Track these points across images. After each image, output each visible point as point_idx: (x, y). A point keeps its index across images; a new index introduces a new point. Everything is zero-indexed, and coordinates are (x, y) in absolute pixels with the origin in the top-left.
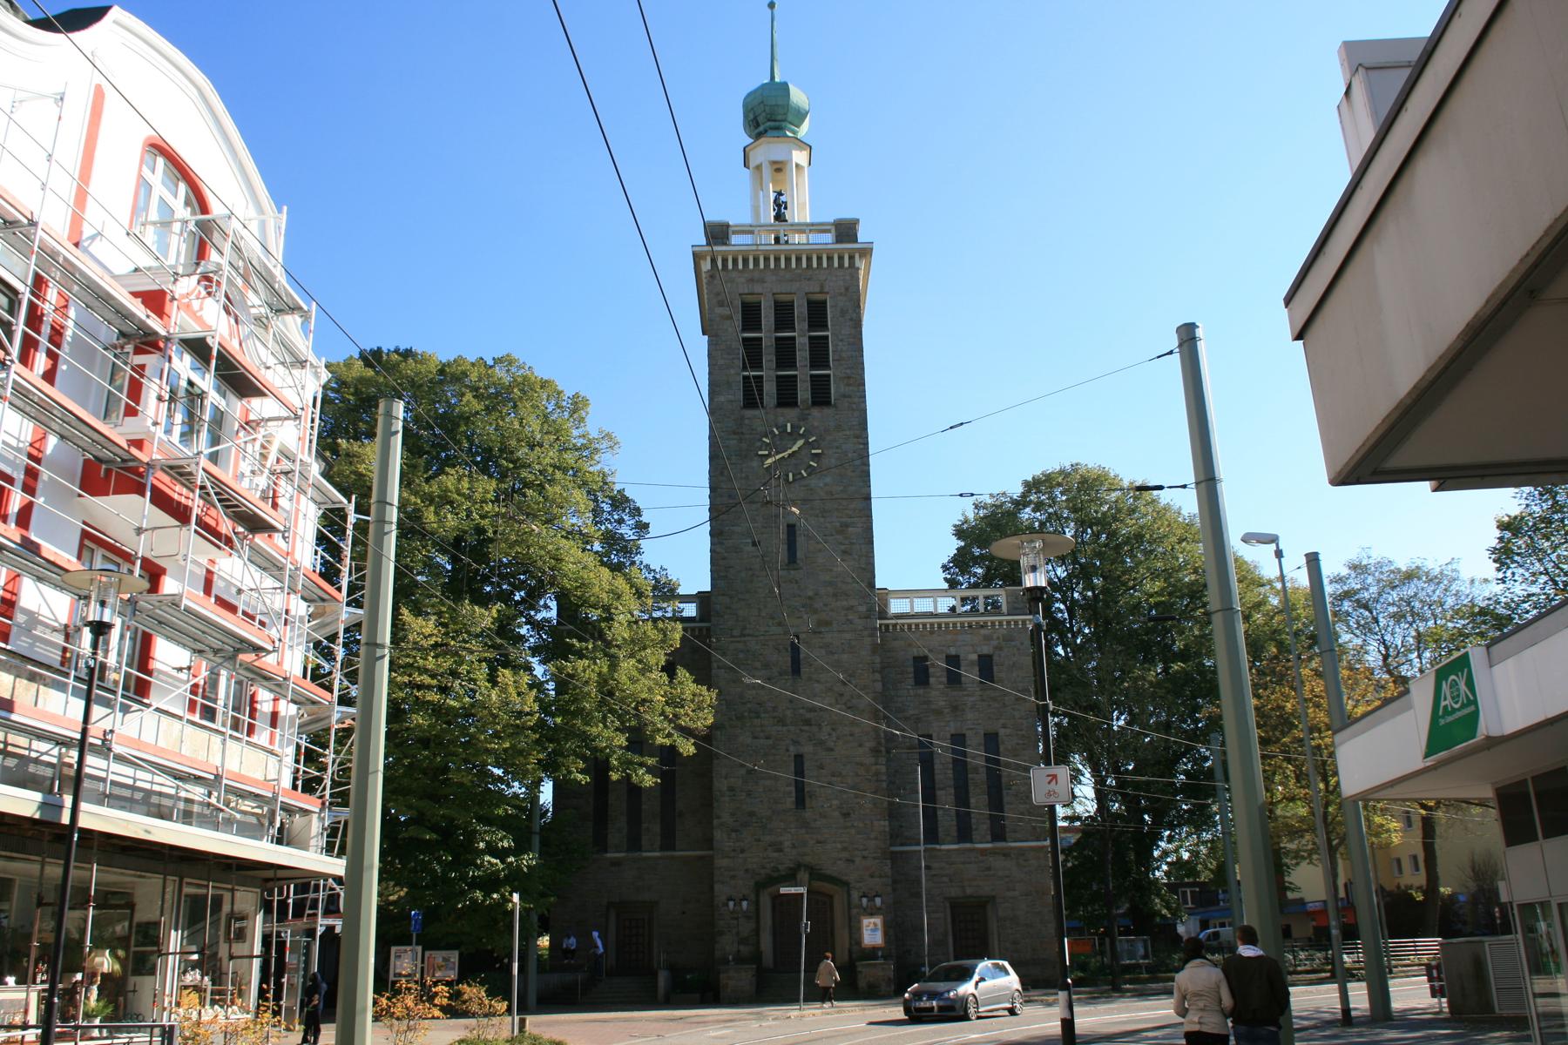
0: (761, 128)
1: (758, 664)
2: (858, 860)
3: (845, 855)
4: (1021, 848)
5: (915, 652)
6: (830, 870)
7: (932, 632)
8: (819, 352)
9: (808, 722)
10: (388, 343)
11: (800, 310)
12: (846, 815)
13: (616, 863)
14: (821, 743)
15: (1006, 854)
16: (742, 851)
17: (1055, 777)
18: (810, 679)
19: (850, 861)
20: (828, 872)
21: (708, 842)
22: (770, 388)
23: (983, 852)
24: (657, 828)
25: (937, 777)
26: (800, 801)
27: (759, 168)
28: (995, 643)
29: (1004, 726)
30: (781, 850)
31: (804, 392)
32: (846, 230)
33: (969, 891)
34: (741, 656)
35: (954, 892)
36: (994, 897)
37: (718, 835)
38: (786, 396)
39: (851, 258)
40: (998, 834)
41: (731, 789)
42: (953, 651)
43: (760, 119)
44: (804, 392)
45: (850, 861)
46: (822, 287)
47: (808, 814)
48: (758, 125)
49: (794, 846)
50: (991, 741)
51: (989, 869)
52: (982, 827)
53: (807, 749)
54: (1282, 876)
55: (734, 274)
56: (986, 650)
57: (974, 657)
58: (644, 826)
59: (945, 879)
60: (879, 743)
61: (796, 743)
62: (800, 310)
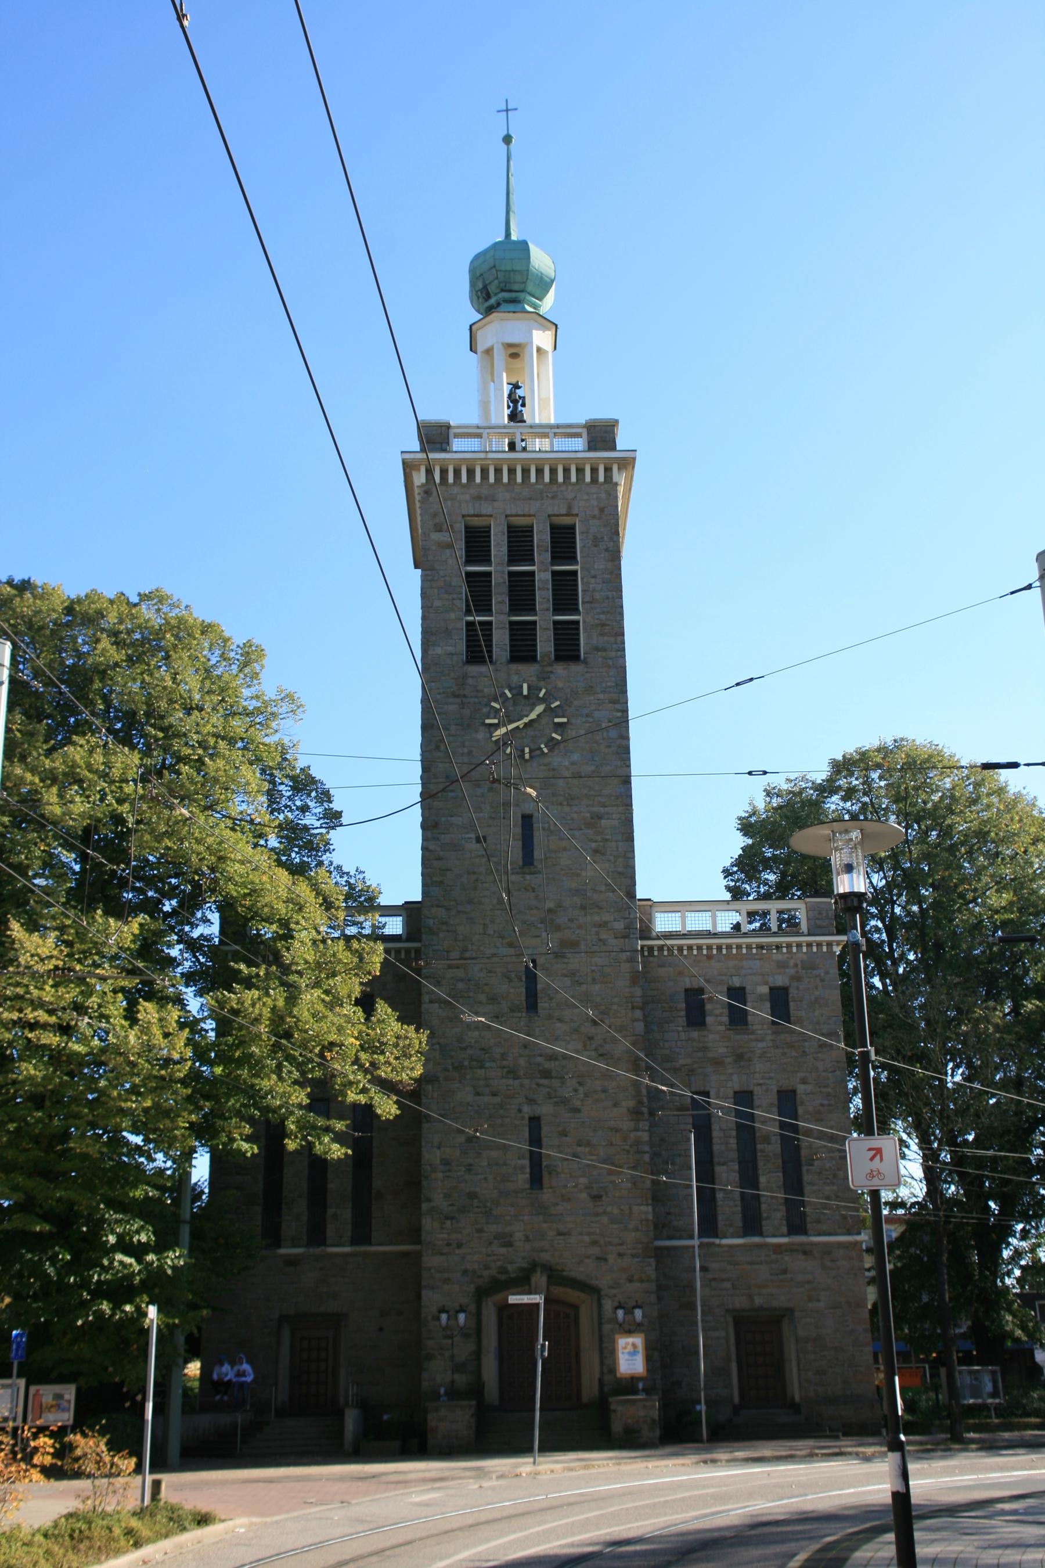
0: (493, 301)
1: (482, 997)
2: (611, 1258)
3: (595, 1251)
5: (688, 983)
7: (709, 957)
8: (565, 591)
9: (546, 1074)
11: (541, 537)
13: (292, 1262)
15: (806, 1251)
16: (460, 1246)
17: (879, 1151)
18: (550, 1017)
20: (573, 1274)
21: (415, 1234)
22: (501, 638)
23: (778, 1249)
24: (347, 1214)
25: (716, 1148)
27: (489, 352)
28: (791, 971)
29: (804, 1081)
30: (509, 1244)
31: (545, 644)
32: (602, 435)
33: (758, 1301)
34: (460, 986)
35: (740, 1302)
36: (791, 1310)
37: (427, 1223)
38: (523, 648)
39: (608, 470)
42: (736, 982)
43: (492, 289)
44: (545, 644)
46: (570, 507)
47: (546, 1196)
48: (488, 297)
49: (527, 1239)
50: (787, 1101)
51: (785, 1271)
53: (545, 1110)
55: (456, 490)
56: (780, 981)
57: (764, 990)
58: (330, 1211)
59: (728, 1285)
60: (640, 1102)
61: (531, 1101)
62: (541, 537)
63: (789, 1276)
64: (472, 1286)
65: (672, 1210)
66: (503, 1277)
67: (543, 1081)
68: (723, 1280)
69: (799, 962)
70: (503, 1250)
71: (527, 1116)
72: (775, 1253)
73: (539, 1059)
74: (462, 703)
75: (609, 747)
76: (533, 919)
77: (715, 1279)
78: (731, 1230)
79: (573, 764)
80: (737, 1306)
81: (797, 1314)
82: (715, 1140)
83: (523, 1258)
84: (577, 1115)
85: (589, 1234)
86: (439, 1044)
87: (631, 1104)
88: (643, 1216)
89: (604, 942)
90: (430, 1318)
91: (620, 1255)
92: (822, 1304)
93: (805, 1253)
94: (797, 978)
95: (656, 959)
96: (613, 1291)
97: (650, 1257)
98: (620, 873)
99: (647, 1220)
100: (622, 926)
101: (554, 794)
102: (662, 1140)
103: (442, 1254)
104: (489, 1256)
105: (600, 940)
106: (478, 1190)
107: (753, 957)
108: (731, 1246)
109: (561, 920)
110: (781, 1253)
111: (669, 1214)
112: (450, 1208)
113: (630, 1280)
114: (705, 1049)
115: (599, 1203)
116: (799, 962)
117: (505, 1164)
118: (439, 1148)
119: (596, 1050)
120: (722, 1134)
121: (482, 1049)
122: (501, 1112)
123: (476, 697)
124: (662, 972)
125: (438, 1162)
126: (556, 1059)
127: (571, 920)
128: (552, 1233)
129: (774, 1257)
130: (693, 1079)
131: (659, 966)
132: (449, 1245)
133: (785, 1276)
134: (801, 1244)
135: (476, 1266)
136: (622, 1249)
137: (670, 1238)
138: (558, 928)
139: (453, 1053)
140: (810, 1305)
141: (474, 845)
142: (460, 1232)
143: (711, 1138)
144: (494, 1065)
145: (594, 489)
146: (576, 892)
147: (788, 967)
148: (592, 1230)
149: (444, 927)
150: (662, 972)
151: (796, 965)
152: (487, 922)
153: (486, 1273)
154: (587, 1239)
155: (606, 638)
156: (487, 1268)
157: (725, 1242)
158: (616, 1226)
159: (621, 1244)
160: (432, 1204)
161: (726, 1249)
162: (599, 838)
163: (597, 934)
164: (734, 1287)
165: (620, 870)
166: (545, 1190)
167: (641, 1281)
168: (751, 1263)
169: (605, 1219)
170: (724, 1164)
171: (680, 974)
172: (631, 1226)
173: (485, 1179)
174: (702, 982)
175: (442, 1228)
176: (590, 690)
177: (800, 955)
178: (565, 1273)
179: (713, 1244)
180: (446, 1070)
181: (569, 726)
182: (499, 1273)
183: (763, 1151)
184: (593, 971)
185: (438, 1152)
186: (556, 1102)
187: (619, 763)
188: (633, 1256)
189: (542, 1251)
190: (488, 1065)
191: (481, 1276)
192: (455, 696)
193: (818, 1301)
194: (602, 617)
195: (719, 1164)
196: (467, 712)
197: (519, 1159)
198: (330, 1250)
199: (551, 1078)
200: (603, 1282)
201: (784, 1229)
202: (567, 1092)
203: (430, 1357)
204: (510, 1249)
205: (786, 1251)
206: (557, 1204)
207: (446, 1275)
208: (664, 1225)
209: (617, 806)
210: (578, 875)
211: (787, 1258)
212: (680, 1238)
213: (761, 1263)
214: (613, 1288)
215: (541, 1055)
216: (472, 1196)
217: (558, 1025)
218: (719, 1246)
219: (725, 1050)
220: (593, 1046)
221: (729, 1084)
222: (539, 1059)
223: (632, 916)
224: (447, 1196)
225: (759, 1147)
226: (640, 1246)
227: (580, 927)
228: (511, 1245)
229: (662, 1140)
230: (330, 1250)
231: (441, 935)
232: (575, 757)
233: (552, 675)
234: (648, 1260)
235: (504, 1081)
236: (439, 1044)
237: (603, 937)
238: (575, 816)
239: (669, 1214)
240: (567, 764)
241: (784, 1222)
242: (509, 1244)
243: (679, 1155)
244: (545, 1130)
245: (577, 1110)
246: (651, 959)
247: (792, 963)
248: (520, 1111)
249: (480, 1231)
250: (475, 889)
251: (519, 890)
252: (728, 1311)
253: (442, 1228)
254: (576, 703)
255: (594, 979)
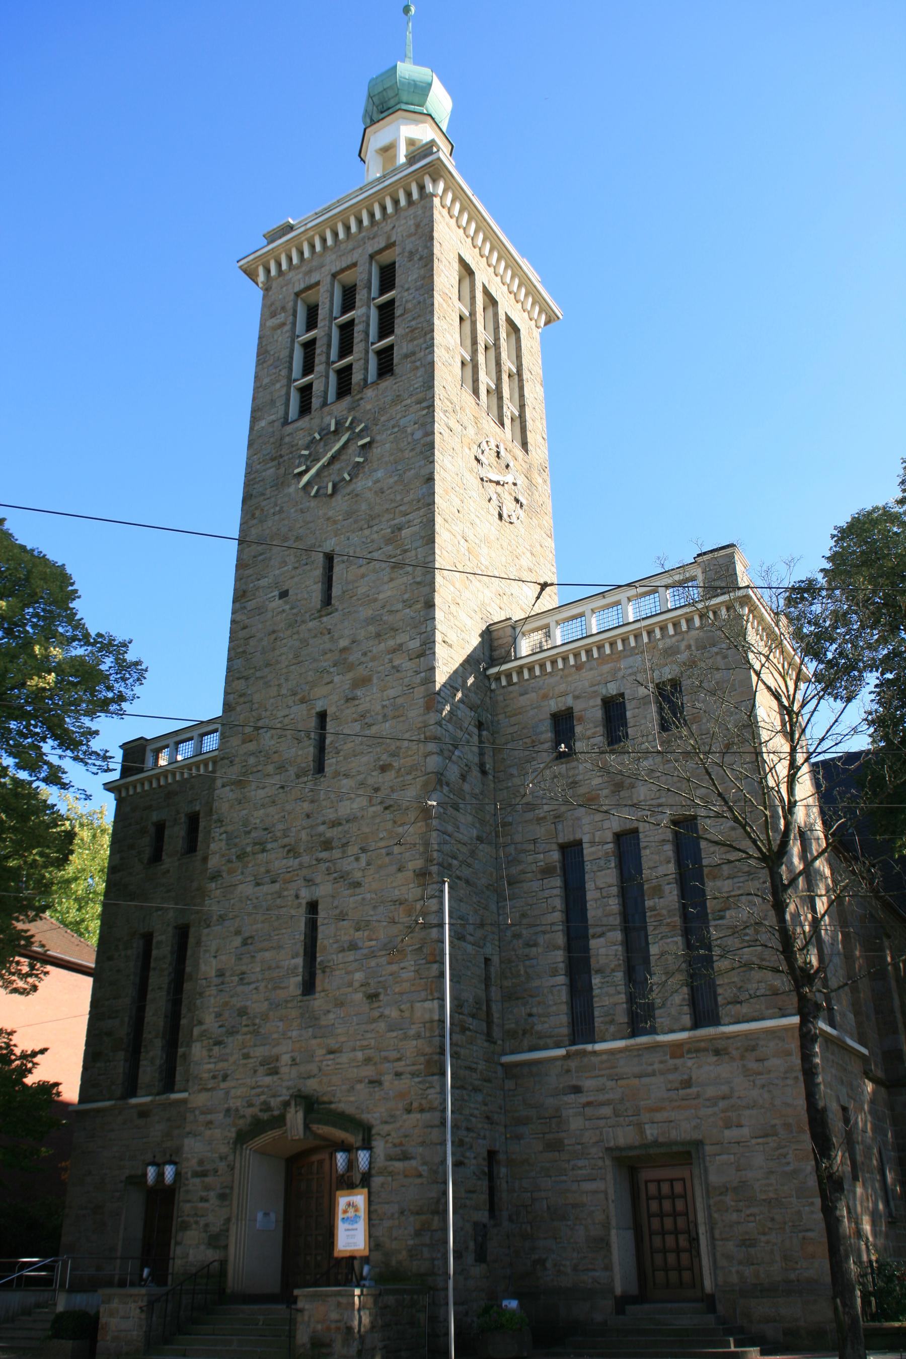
1: (270, 768)
2: (387, 1079)
3: (368, 1072)
4: (747, 1035)
5: (554, 705)
6: (346, 1103)
7: (579, 667)
9: (327, 845)
10: (843, 520)
12: (373, 997)
13: (144, 1113)
14: (344, 876)
15: (719, 1050)
16: (225, 1078)
18: (337, 774)
19: (375, 1082)
20: (341, 1107)
23: (677, 1050)
25: (591, 914)
26: (309, 987)
28: (683, 657)
30: (274, 1072)
33: (651, 1132)
34: (252, 760)
35: (624, 1136)
36: (699, 1144)
40: (703, 1013)
41: (221, 974)
45: (375, 1082)
47: (318, 1002)
49: (294, 1062)
50: (685, 834)
51: (687, 1083)
52: (670, 993)
53: (323, 890)
54: (182, 983)
59: (606, 1111)
60: (429, 861)
61: (310, 882)
63: (694, 1090)
64: (234, 1129)
65: (535, 1010)
66: (265, 1116)
67: (324, 855)
68: (602, 1104)
69: (692, 643)
70: (268, 1080)
71: (304, 902)
72: (673, 1056)
73: (322, 828)
74: (279, 464)
75: (413, 450)
76: (326, 664)
77: (589, 1104)
78: (612, 1029)
79: (377, 481)
80: (621, 1142)
81: (708, 1149)
82: (590, 905)
83: (288, 1088)
84: (358, 890)
85: (363, 1048)
86: (226, 832)
87: (419, 864)
88: (427, 1017)
89: (397, 669)
90: (189, 1175)
91: (398, 1074)
92: (745, 1131)
93: (717, 1052)
94: (692, 664)
95: (516, 687)
96: (387, 1128)
97: (433, 1075)
98: (419, 583)
99: (432, 1021)
100: (418, 644)
101: (356, 522)
102: (524, 915)
103: (208, 1090)
104: (254, 1088)
105: (393, 667)
106: (249, 1003)
107: (632, 652)
108: (611, 1052)
109: (354, 657)
110: (682, 1056)
111: (530, 1015)
112: (220, 1030)
113: (409, 1111)
114: (574, 784)
115: (376, 1005)
116: (692, 643)
117: (278, 967)
118: (215, 957)
119: (381, 803)
120: (598, 895)
121: (266, 829)
122: (279, 901)
123: (291, 453)
124: (523, 701)
125: (213, 973)
126: (340, 824)
127: (365, 654)
128: (321, 1052)
129: (671, 1062)
130: (560, 827)
131: (521, 695)
132: (214, 1077)
133: (688, 1091)
134: (712, 1039)
135: (239, 1103)
136: (400, 1066)
137: (532, 1049)
138: (351, 667)
139: (237, 840)
140: (727, 1133)
141: (278, 602)
142: (227, 1060)
143: (584, 902)
144: (275, 845)
145: (412, 210)
146: (370, 621)
147: (678, 652)
148: (365, 1043)
149: (242, 700)
150: (523, 701)
151: (689, 647)
152: (282, 681)
153: (249, 1112)
154: (360, 1055)
155: (415, 342)
156: (250, 1105)
157: (599, 1047)
158: (394, 1034)
159: (399, 1059)
160: (204, 1027)
161: (604, 1057)
162: (398, 552)
163: (391, 661)
164: (616, 1114)
165: (419, 579)
166: (317, 995)
167: (422, 1110)
168: (639, 1076)
169: (382, 1026)
170: (602, 935)
171: (545, 697)
172: (412, 1032)
173: (256, 989)
174: (570, 701)
175: (210, 1057)
176: (398, 399)
177: (694, 633)
178: (333, 1106)
179: (584, 1053)
180: (230, 861)
181: (375, 445)
182: (261, 1110)
183: (653, 909)
184: (384, 707)
185: (214, 962)
186: (335, 879)
187: (422, 463)
188: (413, 1075)
189: (309, 1078)
190: (269, 846)
191: (244, 1116)
192: (273, 460)
193: (740, 1126)
194: (413, 323)
195: (594, 937)
196: (282, 470)
197: (293, 958)
198: (661, 1038)
199: (332, 849)
200: (374, 1116)
201: (687, 1020)
202: (347, 865)
203: (185, 1226)
204: (275, 1078)
205: (689, 1052)
206: (329, 1012)
207: (209, 1117)
208: (525, 1032)
209: (419, 509)
210: (376, 600)
211: (690, 1063)
212: (546, 1048)
213: (653, 1074)
214: (386, 1122)
215: (324, 823)
216: (242, 1012)
217: (345, 781)
218: (594, 1053)
219: (599, 780)
220: (379, 800)
221: (607, 824)
222: (322, 828)
223: (429, 629)
224: (218, 1015)
225: (648, 903)
226: (422, 1059)
227: (373, 659)
228: (277, 1073)
229: (524, 915)
230: (661, 1038)
231: (238, 709)
232: (380, 474)
233: (362, 402)
234: (430, 1078)
235: (285, 861)
236: (226, 832)
237: (396, 663)
238: (375, 536)
239: (530, 1015)
240: (370, 484)
241: (686, 1009)
242: (274, 1072)
243: (544, 932)
244: (322, 914)
245: (358, 885)
246: (511, 688)
247: (683, 646)
248: (297, 897)
249: (246, 1056)
250: (274, 649)
251: (315, 636)
252: (608, 1149)
253: (210, 1057)
254: (383, 419)
255: (385, 716)
